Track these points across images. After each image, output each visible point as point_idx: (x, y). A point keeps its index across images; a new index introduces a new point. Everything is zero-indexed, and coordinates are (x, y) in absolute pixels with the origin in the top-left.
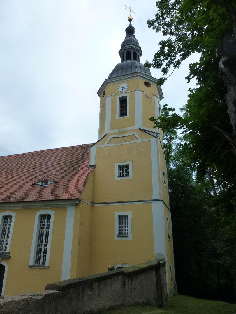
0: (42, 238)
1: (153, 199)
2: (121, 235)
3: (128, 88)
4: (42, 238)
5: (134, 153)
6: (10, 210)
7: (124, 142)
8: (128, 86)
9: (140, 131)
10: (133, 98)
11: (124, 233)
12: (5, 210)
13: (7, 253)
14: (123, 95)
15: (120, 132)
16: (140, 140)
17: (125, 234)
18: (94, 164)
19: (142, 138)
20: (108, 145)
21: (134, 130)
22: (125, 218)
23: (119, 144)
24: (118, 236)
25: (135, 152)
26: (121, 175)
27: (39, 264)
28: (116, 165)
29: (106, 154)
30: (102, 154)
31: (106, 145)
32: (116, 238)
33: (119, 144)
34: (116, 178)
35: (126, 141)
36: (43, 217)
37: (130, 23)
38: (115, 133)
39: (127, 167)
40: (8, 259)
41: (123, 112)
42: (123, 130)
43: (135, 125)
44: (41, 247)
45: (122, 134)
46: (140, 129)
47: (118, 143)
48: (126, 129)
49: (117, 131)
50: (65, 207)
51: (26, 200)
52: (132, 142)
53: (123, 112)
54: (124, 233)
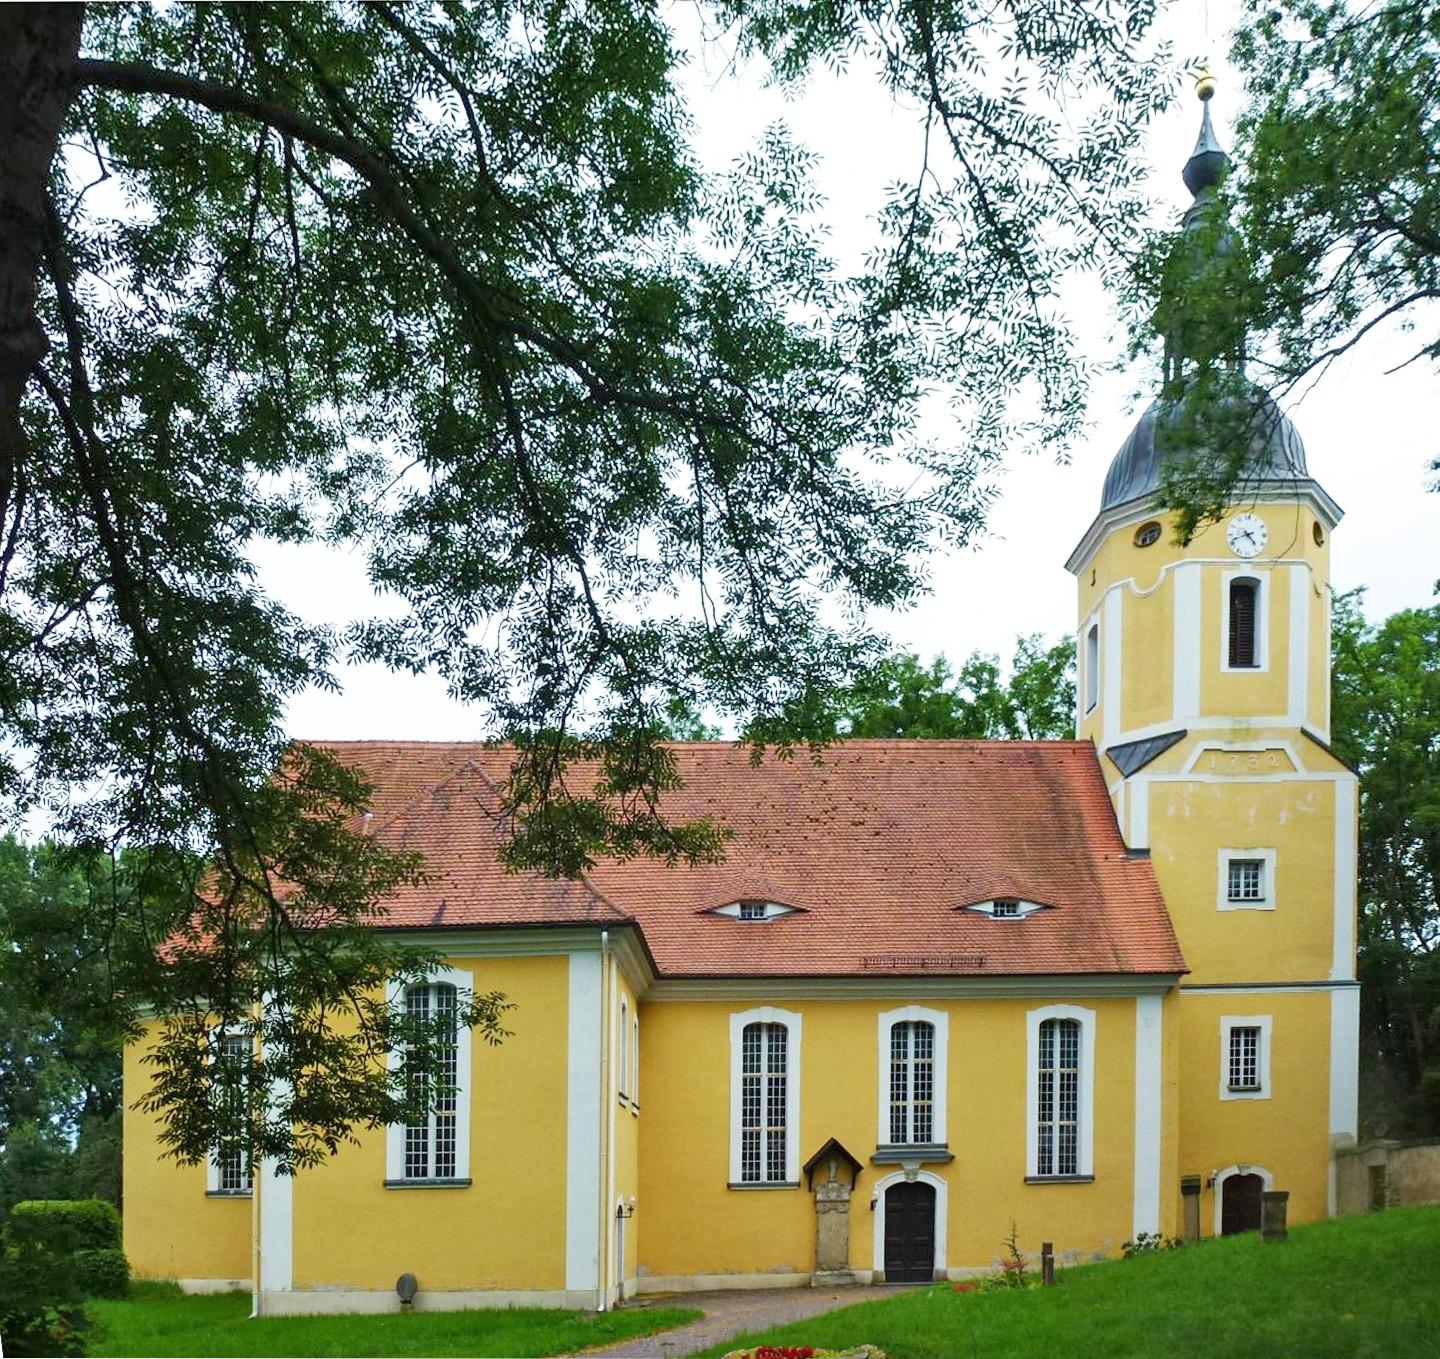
0: (1059, 1096)
1: (1332, 979)
2: (413, 1178)
3: (1265, 540)
4: (1059, 1096)
5: (1283, 821)
6: (923, 1003)
7: (1250, 774)
8: (1264, 531)
9: (1303, 739)
10: (1282, 598)
11: (1242, 1081)
12: (756, 1004)
13: (939, 1146)
14: (1246, 571)
15: (1234, 731)
16: (1302, 774)
17: (1246, 1083)
18: (1145, 847)
19: (1309, 769)
20: (1195, 777)
21: (1282, 733)
22: (1246, 1035)
23: (1231, 780)
24: (1232, 1091)
25: (1284, 815)
26: (1234, 896)
27: (1050, 1172)
28: (1224, 857)
29: (1188, 814)
30: (1171, 812)
31: (1184, 775)
32: (1224, 1094)
33: (1231, 780)
34: (1222, 902)
35: (1252, 772)
36: (899, 1029)
37: (1206, 108)
38: (1217, 734)
39: (1256, 865)
40: (946, 1163)
41: (1242, 651)
42: (1244, 725)
43: (1284, 712)
44: (1065, 1123)
45: (1244, 740)
46: (1304, 732)
47: (1228, 775)
48: (1256, 722)
49: (1226, 724)
50: (1128, 999)
51: (995, 966)
52: (1277, 778)
53: (1242, 651)
54: (1242, 1081)
